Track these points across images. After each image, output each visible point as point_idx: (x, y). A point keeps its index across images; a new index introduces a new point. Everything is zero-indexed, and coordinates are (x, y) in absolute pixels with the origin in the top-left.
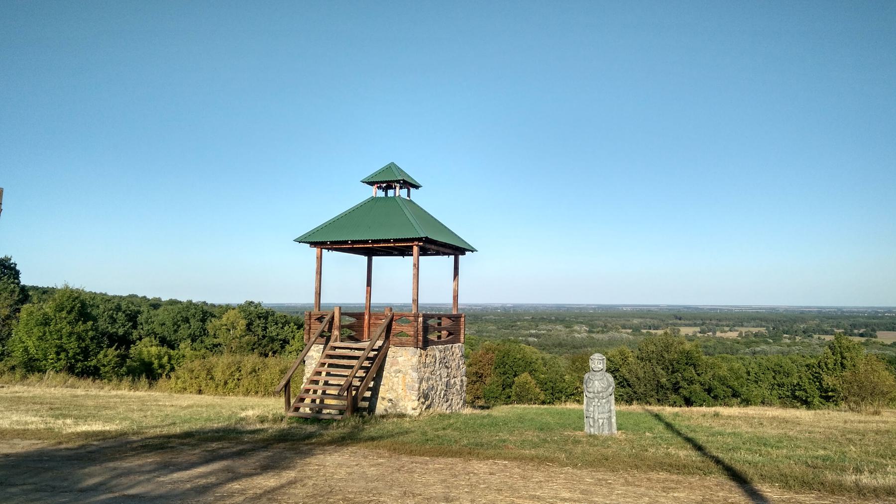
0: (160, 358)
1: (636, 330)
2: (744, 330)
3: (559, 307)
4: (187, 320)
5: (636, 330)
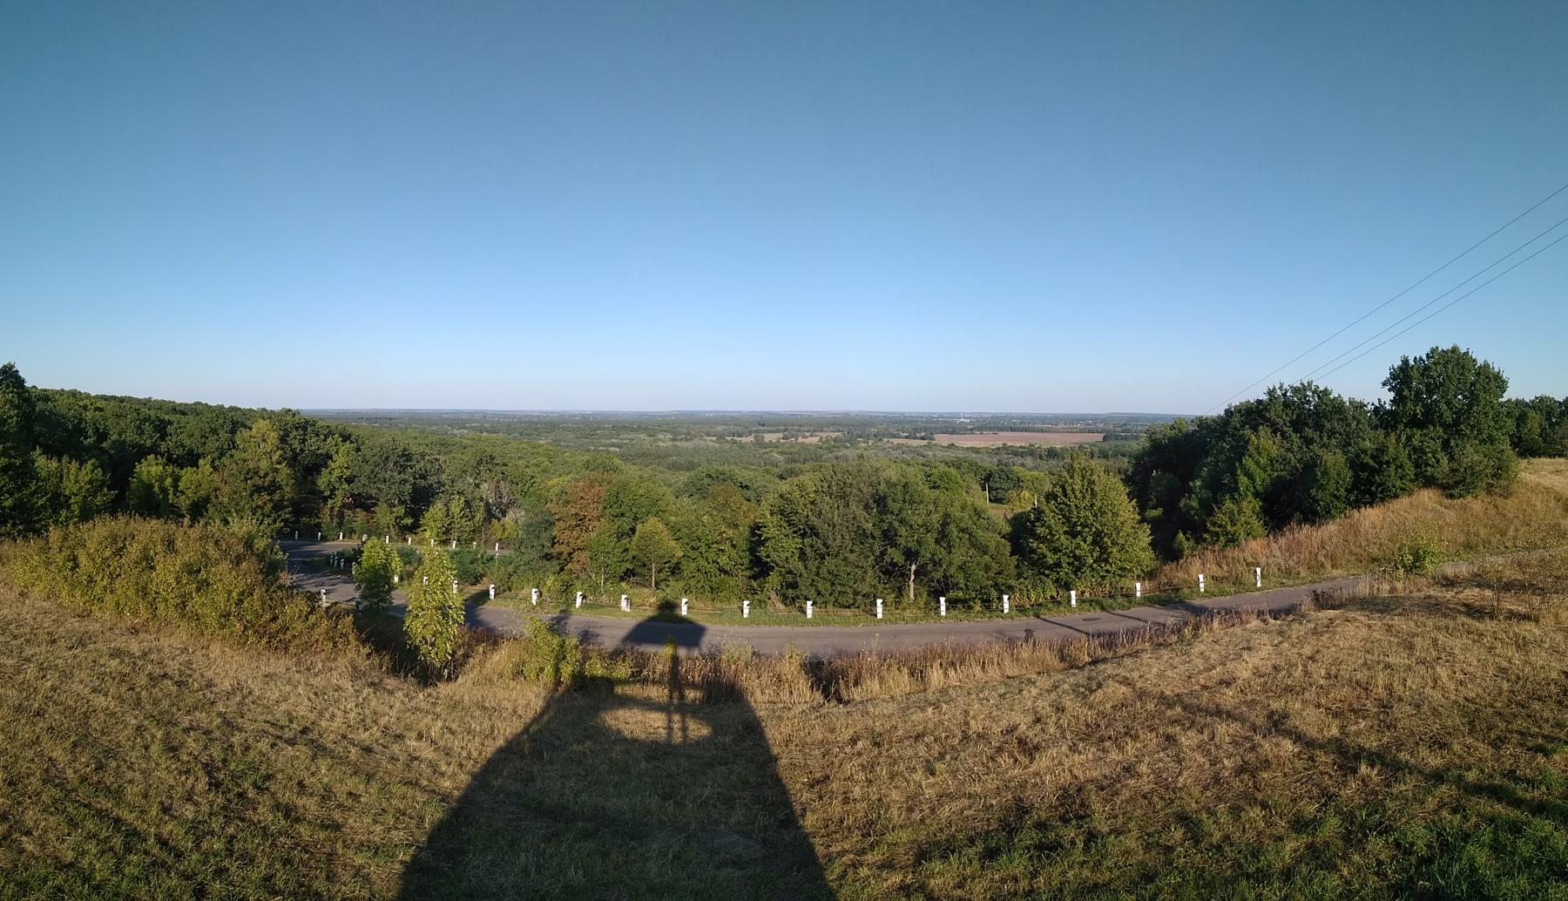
0: (161, 479)
1: (720, 437)
2: (824, 435)
3: (641, 415)
4: (214, 431)
5: (720, 437)
